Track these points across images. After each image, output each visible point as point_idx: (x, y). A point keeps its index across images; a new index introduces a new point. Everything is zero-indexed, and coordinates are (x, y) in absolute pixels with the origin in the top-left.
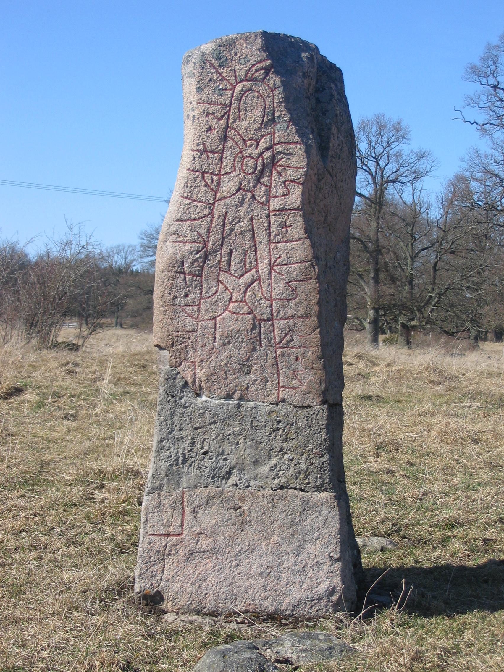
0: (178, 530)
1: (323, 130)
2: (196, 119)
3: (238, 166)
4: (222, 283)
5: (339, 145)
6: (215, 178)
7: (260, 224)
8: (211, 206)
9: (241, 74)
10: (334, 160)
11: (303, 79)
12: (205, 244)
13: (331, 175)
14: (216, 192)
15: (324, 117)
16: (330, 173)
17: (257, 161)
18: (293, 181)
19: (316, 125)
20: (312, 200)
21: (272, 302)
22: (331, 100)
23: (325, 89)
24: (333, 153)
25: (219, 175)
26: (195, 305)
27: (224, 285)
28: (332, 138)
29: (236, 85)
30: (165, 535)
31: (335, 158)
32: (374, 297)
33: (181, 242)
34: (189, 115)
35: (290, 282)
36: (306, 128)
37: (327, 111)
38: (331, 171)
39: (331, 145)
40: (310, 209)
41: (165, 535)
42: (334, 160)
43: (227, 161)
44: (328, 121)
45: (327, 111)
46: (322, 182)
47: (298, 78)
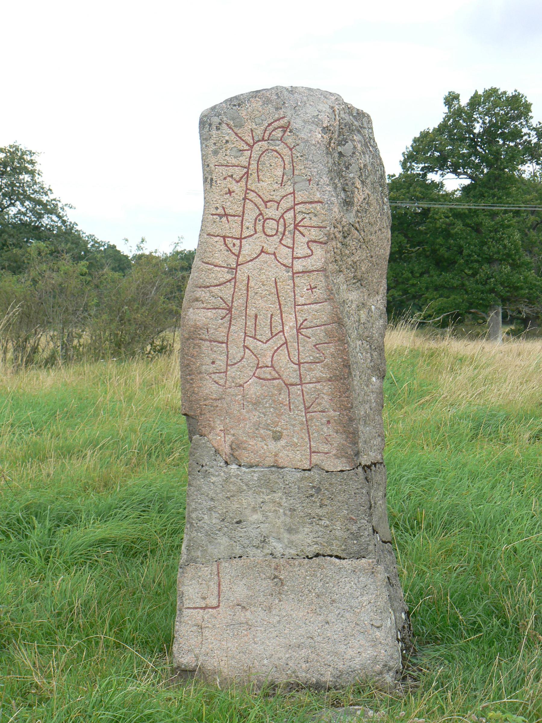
0: (214, 603)
1: (347, 184)
2: (214, 181)
3: (259, 228)
4: (248, 348)
5: (364, 199)
6: (237, 242)
7: (286, 287)
8: (233, 270)
9: (259, 132)
10: (359, 214)
11: (323, 135)
12: (230, 310)
13: (358, 231)
14: (238, 256)
15: (348, 171)
16: (356, 229)
17: (278, 222)
18: (315, 242)
19: (339, 180)
20: (338, 257)
21: (299, 366)
22: (354, 153)
23: (348, 142)
24: (359, 208)
25: (241, 239)
26: (221, 373)
27: (250, 350)
28: (356, 193)
29: (253, 145)
30: (201, 608)
31: (360, 212)
32: (482, 281)
33: (204, 308)
34: (207, 178)
35: (317, 345)
36: (328, 185)
37: (351, 165)
38: (358, 227)
39: (356, 200)
40: (337, 267)
41: (201, 608)
42: (359, 214)
43: (249, 223)
44: (351, 175)
45: (351, 165)
46: (348, 239)
47: (317, 133)
